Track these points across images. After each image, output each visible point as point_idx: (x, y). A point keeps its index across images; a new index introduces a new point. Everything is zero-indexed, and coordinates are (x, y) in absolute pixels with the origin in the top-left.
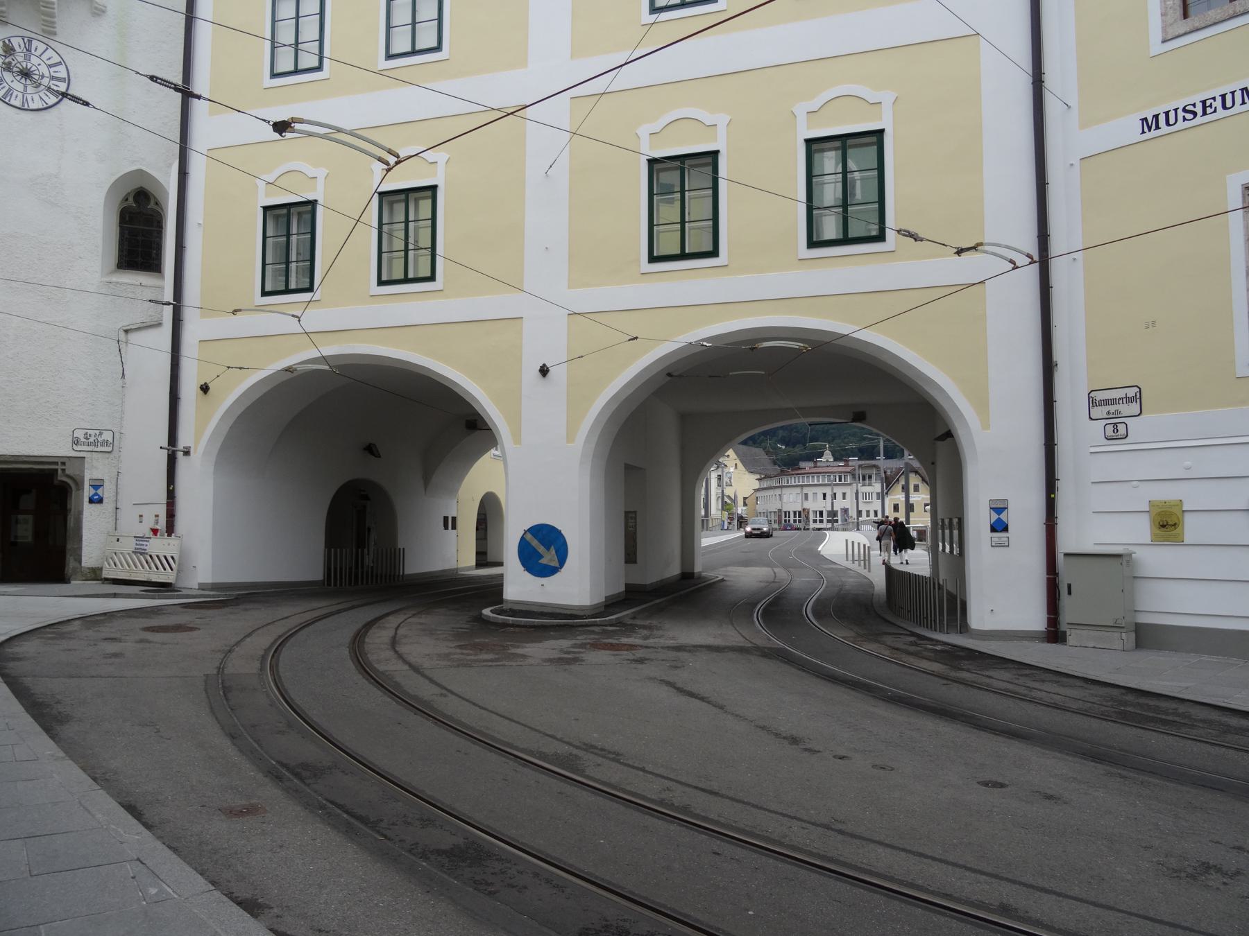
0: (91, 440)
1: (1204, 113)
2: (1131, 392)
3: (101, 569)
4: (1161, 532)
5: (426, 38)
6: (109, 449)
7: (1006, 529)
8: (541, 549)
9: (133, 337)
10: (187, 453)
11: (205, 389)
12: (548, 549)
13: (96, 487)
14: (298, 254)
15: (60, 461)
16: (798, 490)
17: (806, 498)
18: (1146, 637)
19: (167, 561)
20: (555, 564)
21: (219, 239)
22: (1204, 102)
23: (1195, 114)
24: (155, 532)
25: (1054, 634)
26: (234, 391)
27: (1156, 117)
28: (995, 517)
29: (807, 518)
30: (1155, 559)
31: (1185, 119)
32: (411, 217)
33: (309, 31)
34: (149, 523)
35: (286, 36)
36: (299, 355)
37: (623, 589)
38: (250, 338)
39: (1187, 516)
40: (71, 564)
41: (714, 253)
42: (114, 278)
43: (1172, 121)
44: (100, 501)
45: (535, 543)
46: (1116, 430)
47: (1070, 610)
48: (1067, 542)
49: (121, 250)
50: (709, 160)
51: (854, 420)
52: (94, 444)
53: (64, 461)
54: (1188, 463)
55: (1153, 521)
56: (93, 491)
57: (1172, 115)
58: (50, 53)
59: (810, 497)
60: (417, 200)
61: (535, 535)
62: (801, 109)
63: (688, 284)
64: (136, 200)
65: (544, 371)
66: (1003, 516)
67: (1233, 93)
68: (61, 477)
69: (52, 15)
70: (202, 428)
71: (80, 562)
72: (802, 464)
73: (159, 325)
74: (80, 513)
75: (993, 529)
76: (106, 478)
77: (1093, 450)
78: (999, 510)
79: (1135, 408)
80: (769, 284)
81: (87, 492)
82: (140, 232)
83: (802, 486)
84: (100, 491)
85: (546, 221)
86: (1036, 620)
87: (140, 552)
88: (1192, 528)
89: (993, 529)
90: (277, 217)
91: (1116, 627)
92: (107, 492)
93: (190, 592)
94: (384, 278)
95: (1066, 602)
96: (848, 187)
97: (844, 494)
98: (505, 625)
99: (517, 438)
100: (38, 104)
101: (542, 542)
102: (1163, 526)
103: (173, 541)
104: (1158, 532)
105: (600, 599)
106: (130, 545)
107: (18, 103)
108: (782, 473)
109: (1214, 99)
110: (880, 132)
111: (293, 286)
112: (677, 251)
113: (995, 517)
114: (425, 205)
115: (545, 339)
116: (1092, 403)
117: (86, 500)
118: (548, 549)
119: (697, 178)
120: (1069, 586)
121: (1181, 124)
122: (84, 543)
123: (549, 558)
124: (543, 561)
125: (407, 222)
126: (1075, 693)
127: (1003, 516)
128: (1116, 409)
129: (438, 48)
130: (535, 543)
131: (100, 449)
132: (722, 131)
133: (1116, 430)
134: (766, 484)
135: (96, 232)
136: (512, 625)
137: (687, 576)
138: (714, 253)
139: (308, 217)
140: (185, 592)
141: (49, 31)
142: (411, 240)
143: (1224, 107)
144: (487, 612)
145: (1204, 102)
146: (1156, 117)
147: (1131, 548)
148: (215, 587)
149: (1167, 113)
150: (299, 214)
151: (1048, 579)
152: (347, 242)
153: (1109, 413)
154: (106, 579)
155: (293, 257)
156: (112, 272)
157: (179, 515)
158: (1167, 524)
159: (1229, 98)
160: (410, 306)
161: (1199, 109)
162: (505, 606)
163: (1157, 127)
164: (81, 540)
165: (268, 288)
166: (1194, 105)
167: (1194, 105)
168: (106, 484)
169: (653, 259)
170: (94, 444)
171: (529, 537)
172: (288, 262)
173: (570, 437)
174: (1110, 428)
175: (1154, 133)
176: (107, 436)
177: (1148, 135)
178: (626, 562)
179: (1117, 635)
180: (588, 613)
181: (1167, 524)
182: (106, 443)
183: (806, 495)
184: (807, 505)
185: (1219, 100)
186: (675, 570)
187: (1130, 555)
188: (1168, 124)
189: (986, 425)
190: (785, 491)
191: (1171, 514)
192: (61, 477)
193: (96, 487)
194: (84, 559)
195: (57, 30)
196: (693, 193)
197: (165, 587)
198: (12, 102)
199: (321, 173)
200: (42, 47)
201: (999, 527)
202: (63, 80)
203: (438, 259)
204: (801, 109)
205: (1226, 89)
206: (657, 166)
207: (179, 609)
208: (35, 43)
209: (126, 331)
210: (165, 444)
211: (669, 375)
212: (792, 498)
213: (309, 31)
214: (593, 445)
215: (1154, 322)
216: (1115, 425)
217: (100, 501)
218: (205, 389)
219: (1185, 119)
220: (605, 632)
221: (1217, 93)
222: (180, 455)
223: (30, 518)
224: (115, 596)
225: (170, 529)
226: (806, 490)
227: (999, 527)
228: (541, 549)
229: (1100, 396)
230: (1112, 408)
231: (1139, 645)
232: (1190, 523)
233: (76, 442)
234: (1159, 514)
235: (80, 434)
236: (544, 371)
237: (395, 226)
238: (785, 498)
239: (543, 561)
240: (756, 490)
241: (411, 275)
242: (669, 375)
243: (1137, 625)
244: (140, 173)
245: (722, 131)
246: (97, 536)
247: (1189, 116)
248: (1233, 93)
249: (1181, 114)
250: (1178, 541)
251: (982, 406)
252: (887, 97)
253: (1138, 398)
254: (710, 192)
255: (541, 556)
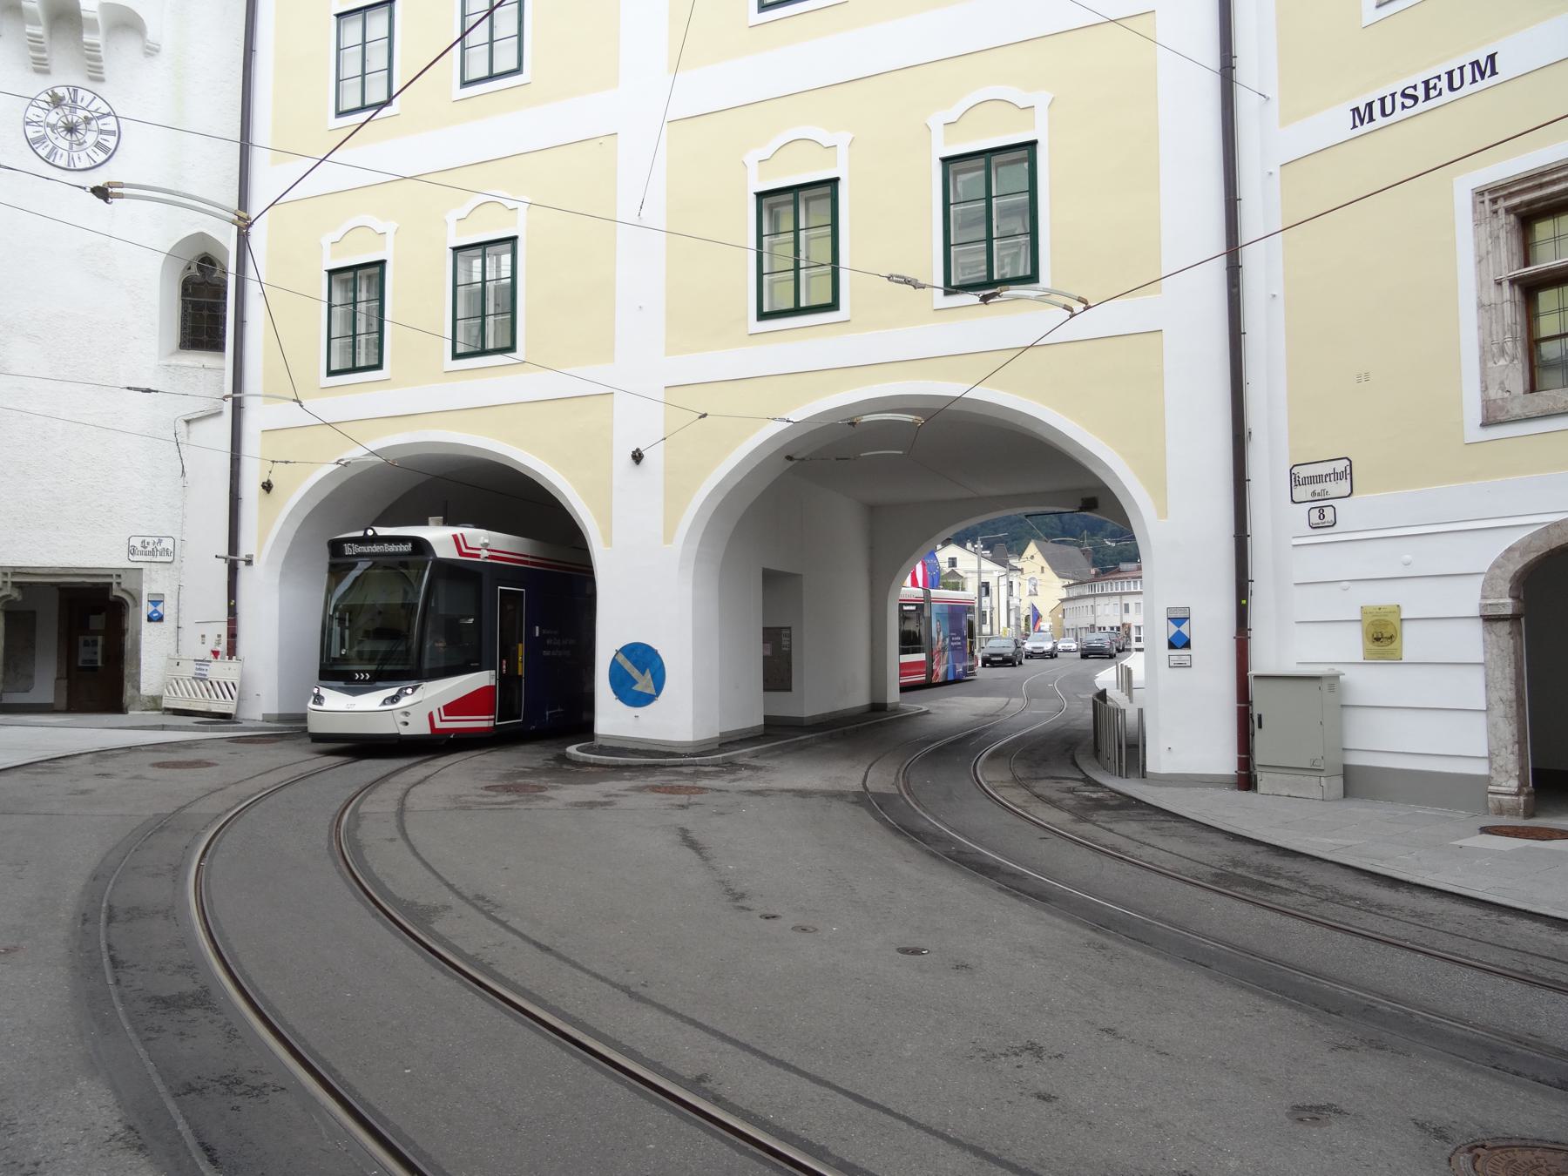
0: (150, 548)
1: (1427, 97)
2: (1341, 466)
3: (161, 698)
4: (1374, 647)
5: (505, 61)
6: (169, 559)
7: (1187, 645)
8: (635, 673)
9: (195, 427)
10: (249, 562)
11: (267, 487)
12: (643, 673)
13: (155, 603)
14: (496, 305)
15: (114, 573)
16: (1116, 599)
17: (1127, 610)
18: (1356, 783)
19: (227, 688)
20: (651, 690)
21: (283, 314)
22: (1426, 83)
23: (1416, 99)
24: (216, 653)
25: (1246, 780)
26: (303, 484)
27: (1370, 105)
28: (1174, 629)
29: (1128, 636)
30: (1369, 682)
31: (1404, 107)
32: (802, 225)
33: (377, 60)
34: (211, 644)
35: (352, 67)
36: (362, 449)
37: (762, 722)
38: (325, 425)
39: (1406, 625)
40: (129, 692)
41: (833, 306)
42: (174, 361)
43: (1388, 110)
44: (160, 619)
45: (628, 666)
46: (1322, 515)
47: (1262, 752)
48: (1263, 661)
49: (183, 328)
50: (1024, 153)
51: (1082, 509)
52: (153, 553)
53: (119, 573)
54: (1407, 557)
55: (1365, 633)
56: (152, 608)
57: (1388, 101)
58: (98, 103)
59: (1132, 608)
60: (498, 255)
61: (628, 657)
62: (936, 120)
63: (359, 398)
64: (199, 267)
65: (637, 457)
66: (1184, 629)
67: (1461, 68)
68: (116, 592)
69: (99, 59)
70: (267, 530)
71: (138, 689)
72: (1123, 566)
73: (219, 413)
74: (139, 633)
75: (1172, 646)
76: (167, 593)
77: (1295, 542)
78: (1179, 621)
79: (1343, 487)
80: (901, 345)
81: (146, 608)
82: (204, 308)
83: (1121, 594)
84: (159, 608)
85: (640, 273)
86: (1225, 762)
87: (201, 678)
88: (1412, 641)
89: (1172, 646)
90: (345, 282)
91: (1313, 770)
92: (168, 609)
93: (252, 725)
94: (766, 309)
95: (1260, 740)
96: (993, 213)
97: (1138, 604)
98: (586, 764)
99: (608, 541)
100: (86, 163)
101: (635, 664)
102: (1378, 639)
103: (233, 665)
104: (1371, 646)
105: (712, 730)
106: (190, 669)
107: (63, 163)
108: (1097, 577)
109: (1439, 77)
110: (1032, 145)
111: (490, 345)
112: (791, 305)
113: (1174, 629)
114: (821, 210)
115: (638, 422)
116: (1295, 481)
117: (145, 617)
118: (643, 673)
119: (1009, 178)
120: (1260, 717)
121: (1399, 114)
122: (143, 667)
123: (644, 684)
124: (637, 688)
125: (796, 230)
126: (1178, 846)
127: (1184, 629)
128: (1323, 487)
129: (518, 71)
130: (628, 666)
131: (159, 559)
132: (843, 152)
133: (1322, 515)
134: (1075, 592)
135: (154, 306)
136: (593, 765)
137: (878, 707)
138: (833, 306)
139: (376, 280)
140: (245, 724)
141: (96, 75)
142: (802, 255)
143: (1451, 88)
144: (572, 750)
145: (1426, 83)
146: (1370, 105)
147: (1338, 669)
148: (282, 718)
149: (1382, 100)
150: (369, 277)
151: (1239, 709)
152: (419, 304)
153: (1314, 493)
154: (167, 709)
155: (491, 309)
156: (172, 354)
157: (231, 635)
158: (1382, 636)
159: (1457, 75)
160: (492, 381)
161: (1421, 93)
162: (598, 742)
163: (1371, 119)
164: (139, 665)
165: (461, 349)
166: (1415, 87)
167: (1415, 87)
168: (167, 599)
169: (762, 316)
170: (153, 553)
171: (621, 658)
172: (483, 316)
173: (668, 538)
174: (1315, 513)
175: (1367, 127)
176: (167, 543)
177: (1361, 130)
178: (765, 690)
179: (1315, 780)
180: (689, 751)
181: (1382, 636)
182: (166, 552)
183: (1127, 606)
184: (1127, 619)
185: (1445, 78)
186: (859, 698)
187: (1336, 677)
188: (1383, 114)
189: (1163, 512)
190: (1099, 601)
191: (1387, 624)
192: (116, 592)
193: (155, 603)
194: (142, 686)
195: (106, 75)
196: (812, 232)
197: (226, 716)
198: (57, 162)
199: (390, 227)
200: (89, 96)
201: (1179, 642)
202: (112, 133)
203: (450, 336)
204: (936, 120)
205: (1453, 65)
206: (953, 167)
207: (223, 742)
208: (81, 93)
209: (188, 422)
210: (225, 552)
211: (789, 458)
212: (1108, 610)
213: (377, 60)
214: (695, 546)
215: (1367, 374)
216: (1321, 509)
217: (160, 619)
218: (267, 487)
219: (1404, 107)
220: (681, 773)
221: (1442, 70)
222: (241, 564)
223: (100, 639)
224: (163, 727)
225: (232, 650)
226: (1126, 599)
227: (1179, 642)
228: (635, 673)
229: (1304, 472)
230: (1318, 487)
231: (1347, 793)
232: (1409, 631)
233: (132, 551)
234: (1372, 623)
235: (136, 542)
236: (637, 457)
237: (782, 237)
238: (1099, 610)
239: (637, 688)
240: (1063, 601)
241: (803, 304)
242: (789, 458)
243: (1346, 767)
244: (202, 237)
245: (843, 152)
246: (159, 658)
247: (1409, 102)
248: (1461, 68)
249: (1399, 99)
250: (1395, 658)
251: (1158, 487)
252: (1041, 99)
253: (1348, 474)
254: (829, 229)
255: (635, 682)
